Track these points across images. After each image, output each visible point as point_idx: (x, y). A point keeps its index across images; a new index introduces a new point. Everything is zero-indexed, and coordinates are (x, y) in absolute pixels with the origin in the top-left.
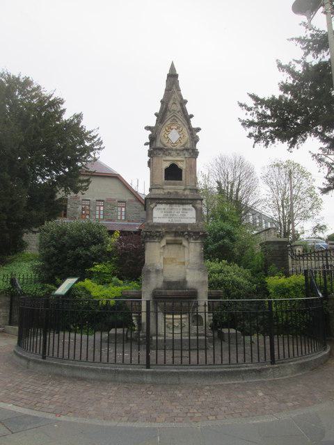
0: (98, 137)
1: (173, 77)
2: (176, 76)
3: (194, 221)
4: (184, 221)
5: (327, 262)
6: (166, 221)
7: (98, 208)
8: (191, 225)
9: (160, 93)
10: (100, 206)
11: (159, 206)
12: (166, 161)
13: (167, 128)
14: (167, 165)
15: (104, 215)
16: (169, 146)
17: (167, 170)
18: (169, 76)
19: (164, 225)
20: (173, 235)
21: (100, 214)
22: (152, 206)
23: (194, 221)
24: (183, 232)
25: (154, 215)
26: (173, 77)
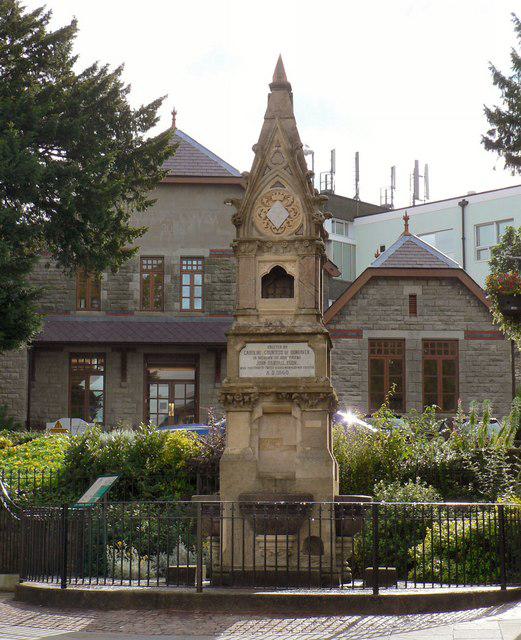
0: (163, 113)
1: (281, 88)
2: (160, 104)
3: (312, 373)
4: (293, 373)
5: (376, 522)
6: (262, 373)
7: (186, 279)
8: (308, 379)
9: (262, 106)
10: (192, 273)
11: (250, 347)
12: (265, 261)
13: (265, 200)
14: (266, 269)
15: (204, 298)
16: (269, 234)
17: (265, 279)
18: (272, 86)
19: (257, 381)
20: (272, 398)
21: (192, 298)
22: (238, 348)
23: (312, 373)
24: (291, 394)
25: (242, 364)
26: (281, 88)
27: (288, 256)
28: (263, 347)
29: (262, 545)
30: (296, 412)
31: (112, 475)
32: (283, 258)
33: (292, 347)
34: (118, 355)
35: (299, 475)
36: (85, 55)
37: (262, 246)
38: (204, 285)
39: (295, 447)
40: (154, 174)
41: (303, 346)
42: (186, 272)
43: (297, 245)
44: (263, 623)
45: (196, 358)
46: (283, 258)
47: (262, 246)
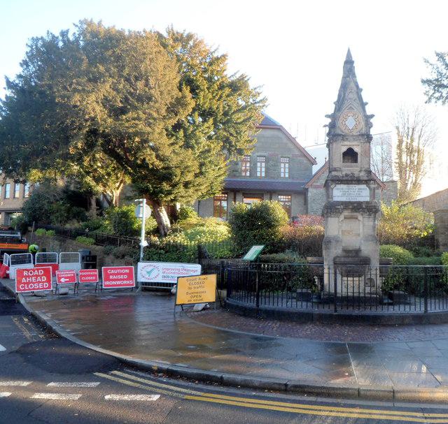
1: (349, 64)
7: (259, 164)
11: (338, 186)
14: (344, 149)
15: (266, 172)
21: (261, 172)
26: (349, 64)
27: (355, 143)
28: (344, 187)
29: (346, 282)
30: (360, 218)
31: (260, 244)
32: (353, 143)
33: (358, 187)
34: (233, 193)
35: (362, 248)
36: (231, 71)
37: (344, 137)
38: (265, 167)
39: (359, 235)
40: (157, 188)
41: (364, 186)
42: (259, 162)
43: (360, 138)
44: (372, 332)
45: (262, 195)
46: (353, 143)
47: (344, 137)
